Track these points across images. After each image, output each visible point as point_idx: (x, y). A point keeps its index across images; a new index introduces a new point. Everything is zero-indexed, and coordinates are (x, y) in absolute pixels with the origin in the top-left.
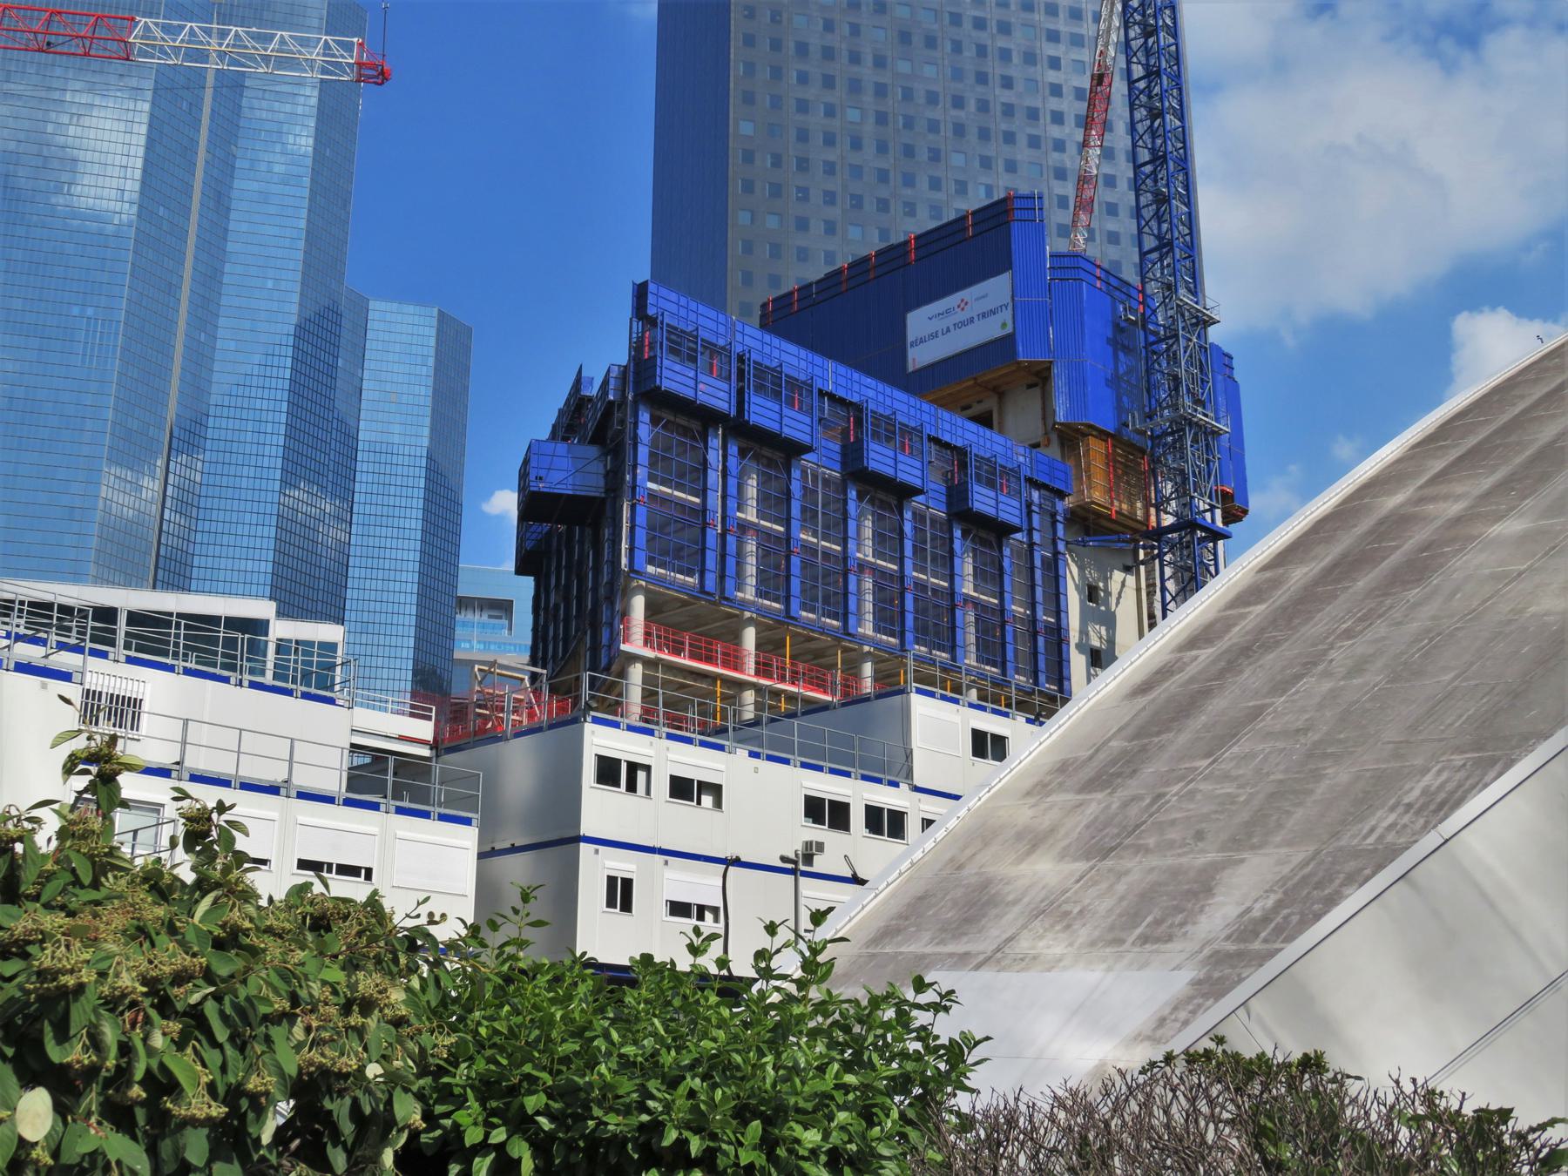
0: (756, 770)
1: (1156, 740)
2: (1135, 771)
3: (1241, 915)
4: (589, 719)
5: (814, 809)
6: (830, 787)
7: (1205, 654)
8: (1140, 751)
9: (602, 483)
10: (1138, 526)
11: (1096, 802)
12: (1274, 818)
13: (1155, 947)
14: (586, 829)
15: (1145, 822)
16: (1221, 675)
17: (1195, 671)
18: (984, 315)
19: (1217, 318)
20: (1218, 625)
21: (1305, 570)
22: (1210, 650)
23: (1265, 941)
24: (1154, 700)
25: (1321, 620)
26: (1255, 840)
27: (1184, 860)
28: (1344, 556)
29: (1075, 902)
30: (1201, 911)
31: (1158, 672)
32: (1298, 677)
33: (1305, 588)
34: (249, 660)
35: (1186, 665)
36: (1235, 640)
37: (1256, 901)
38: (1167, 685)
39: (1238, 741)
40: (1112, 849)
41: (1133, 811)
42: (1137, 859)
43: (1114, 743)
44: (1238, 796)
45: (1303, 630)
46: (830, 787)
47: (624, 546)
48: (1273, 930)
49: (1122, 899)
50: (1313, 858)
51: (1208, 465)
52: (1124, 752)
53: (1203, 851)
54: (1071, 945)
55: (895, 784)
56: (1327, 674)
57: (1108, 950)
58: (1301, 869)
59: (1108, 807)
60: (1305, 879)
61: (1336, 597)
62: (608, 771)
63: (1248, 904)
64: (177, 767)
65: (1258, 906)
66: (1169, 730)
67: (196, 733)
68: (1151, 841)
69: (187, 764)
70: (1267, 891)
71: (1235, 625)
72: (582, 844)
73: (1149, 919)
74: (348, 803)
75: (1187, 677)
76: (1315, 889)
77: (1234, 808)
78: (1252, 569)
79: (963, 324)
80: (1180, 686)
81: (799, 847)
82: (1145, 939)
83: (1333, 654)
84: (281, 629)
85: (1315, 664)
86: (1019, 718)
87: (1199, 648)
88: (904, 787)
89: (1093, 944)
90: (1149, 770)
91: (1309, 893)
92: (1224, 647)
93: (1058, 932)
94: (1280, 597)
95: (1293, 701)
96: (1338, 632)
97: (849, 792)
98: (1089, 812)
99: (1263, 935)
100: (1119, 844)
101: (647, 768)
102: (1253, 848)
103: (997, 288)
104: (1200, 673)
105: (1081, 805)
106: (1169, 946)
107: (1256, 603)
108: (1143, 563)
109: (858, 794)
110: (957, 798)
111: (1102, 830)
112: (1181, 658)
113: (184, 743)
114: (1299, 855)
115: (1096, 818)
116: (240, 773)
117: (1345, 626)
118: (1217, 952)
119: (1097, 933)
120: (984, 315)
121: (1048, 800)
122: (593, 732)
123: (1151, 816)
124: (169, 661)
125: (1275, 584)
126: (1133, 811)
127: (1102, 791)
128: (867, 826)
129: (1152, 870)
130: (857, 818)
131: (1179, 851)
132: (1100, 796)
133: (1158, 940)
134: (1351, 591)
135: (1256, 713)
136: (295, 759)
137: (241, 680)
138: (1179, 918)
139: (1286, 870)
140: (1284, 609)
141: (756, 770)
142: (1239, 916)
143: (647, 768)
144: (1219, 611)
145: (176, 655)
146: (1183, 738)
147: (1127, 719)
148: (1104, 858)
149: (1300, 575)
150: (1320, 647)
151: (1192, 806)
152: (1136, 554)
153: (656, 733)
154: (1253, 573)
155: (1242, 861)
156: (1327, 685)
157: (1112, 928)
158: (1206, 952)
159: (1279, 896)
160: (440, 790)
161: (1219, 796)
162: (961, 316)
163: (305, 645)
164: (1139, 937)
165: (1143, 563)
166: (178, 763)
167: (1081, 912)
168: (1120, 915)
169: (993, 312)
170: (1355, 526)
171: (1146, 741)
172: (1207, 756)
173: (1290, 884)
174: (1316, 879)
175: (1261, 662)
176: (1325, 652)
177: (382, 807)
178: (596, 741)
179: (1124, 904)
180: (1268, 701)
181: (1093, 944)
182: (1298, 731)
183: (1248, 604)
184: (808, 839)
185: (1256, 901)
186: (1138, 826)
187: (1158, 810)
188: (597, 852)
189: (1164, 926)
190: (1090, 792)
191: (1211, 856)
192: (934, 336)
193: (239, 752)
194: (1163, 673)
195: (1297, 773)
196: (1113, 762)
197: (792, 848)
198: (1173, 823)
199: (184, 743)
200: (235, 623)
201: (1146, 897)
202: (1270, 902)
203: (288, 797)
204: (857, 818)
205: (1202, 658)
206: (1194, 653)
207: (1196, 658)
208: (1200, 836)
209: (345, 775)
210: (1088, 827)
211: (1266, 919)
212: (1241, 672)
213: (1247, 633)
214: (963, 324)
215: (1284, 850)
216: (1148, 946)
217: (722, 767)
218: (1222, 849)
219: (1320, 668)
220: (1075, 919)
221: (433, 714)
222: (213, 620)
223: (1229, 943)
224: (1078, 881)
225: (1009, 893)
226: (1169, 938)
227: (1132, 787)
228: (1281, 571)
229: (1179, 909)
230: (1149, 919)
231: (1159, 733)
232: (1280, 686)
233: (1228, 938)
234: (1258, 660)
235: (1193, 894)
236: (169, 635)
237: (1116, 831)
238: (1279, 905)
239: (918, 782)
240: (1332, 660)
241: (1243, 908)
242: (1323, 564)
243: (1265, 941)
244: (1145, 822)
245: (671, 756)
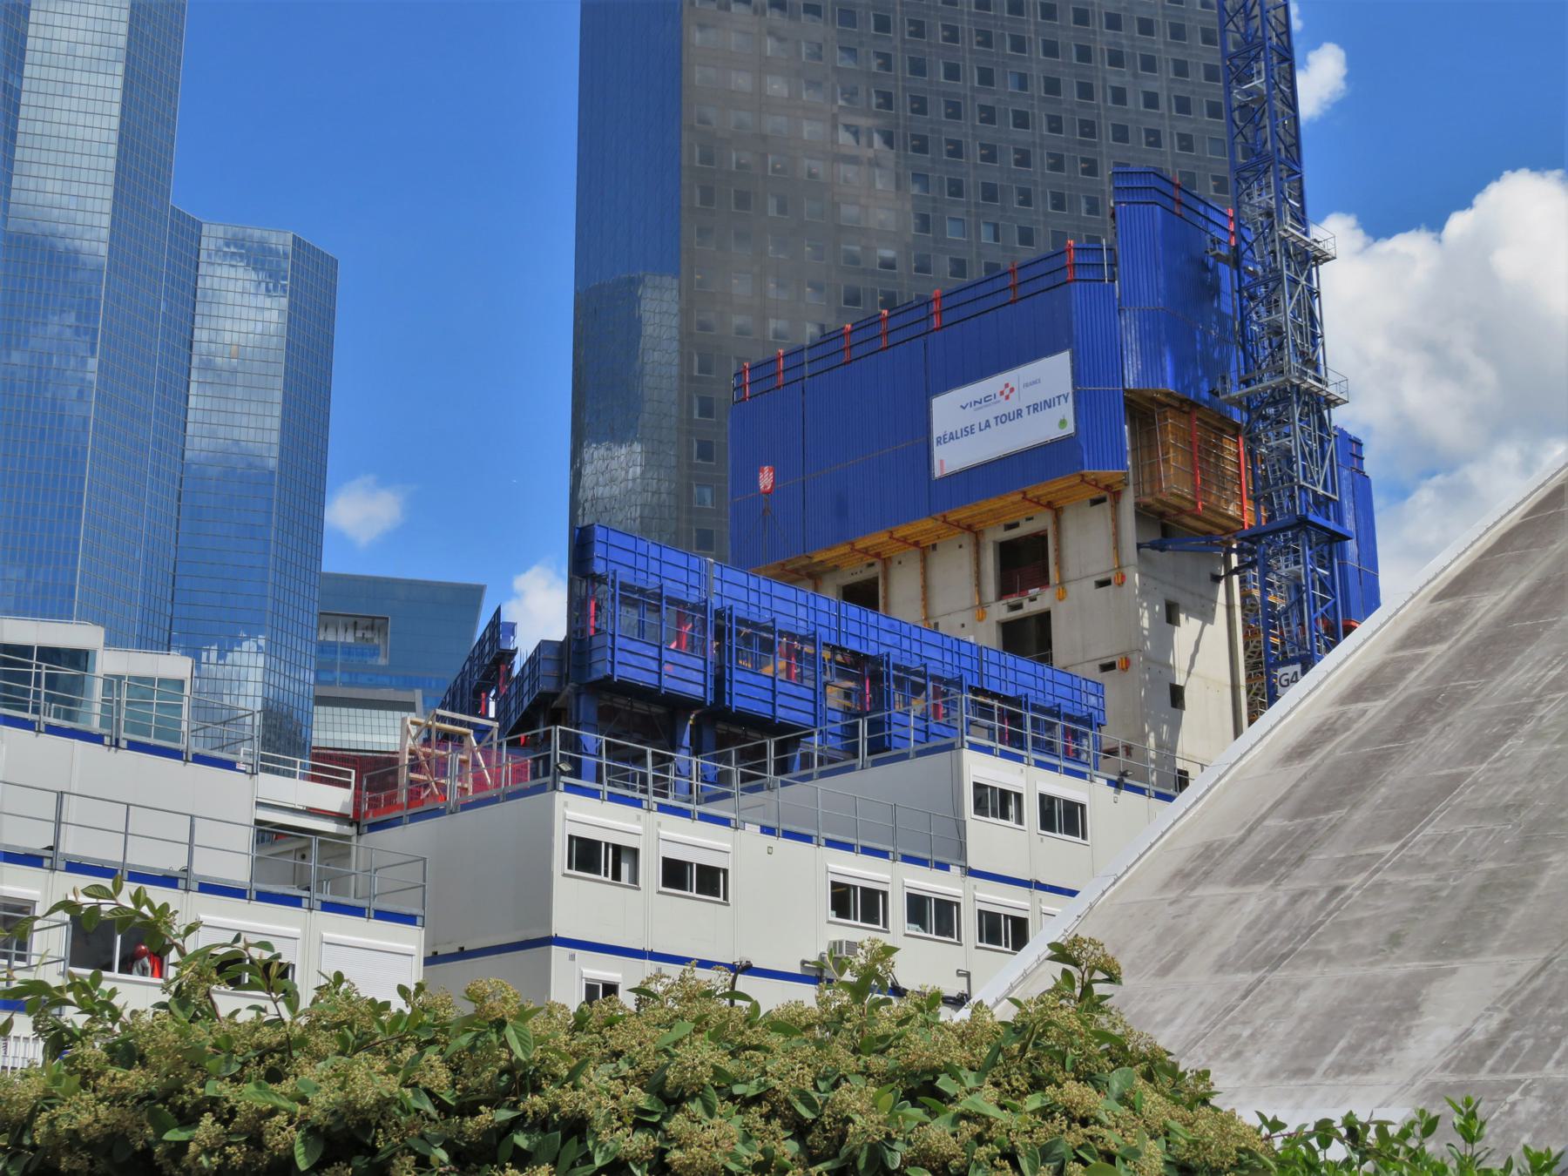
0: (770, 851)
1: (1325, 818)
2: (1302, 858)
3: (1460, 1038)
4: (561, 787)
5: (842, 899)
6: (860, 870)
7: (1376, 708)
8: (1304, 833)
10: (1232, 524)
11: (1256, 899)
12: (1489, 917)
13: (1353, 1078)
14: (559, 928)
15: (1322, 923)
16: (1400, 734)
17: (1365, 729)
18: (1036, 408)
19: (1332, 252)
20: (1388, 670)
21: (1495, 598)
22: (1381, 703)
23: (1493, 1070)
24: (1316, 767)
25: (1521, 665)
26: (1467, 945)
27: (1378, 970)
28: (1544, 582)
29: (1244, 1023)
30: (1408, 1033)
31: (1316, 731)
32: (1502, 738)
33: (1497, 624)
34: (50, 698)
35: (1351, 721)
36: (1413, 690)
37: (1476, 1021)
38: (1329, 747)
39: (1432, 820)
40: (1284, 957)
41: (1306, 906)
42: (1318, 969)
43: (1269, 822)
44: (1440, 890)
45: (1499, 678)
48: (1503, 1056)
49: (1303, 1019)
50: (1543, 968)
51: (1322, 446)
52: (1284, 834)
53: (1401, 959)
54: (1244, 1076)
55: (944, 867)
56: (1536, 736)
57: (1293, 1082)
58: (1530, 981)
59: (1273, 902)
60: (1536, 993)
61: (1538, 635)
62: (586, 855)
63: (1465, 1026)
64: (49, 853)
65: (1480, 1027)
66: (1339, 805)
67: (74, 809)
68: (1333, 947)
69: (61, 850)
70: (1488, 1009)
71: (1410, 669)
72: (554, 947)
73: (1342, 1044)
74: (264, 897)
75: (1355, 737)
76: (1550, 1006)
77: (1435, 904)
78: (1426, 596)
79: (1003, 419)
80: (1349, 749)
81: (824, 949)
82: (1339, 1069)
83: (1542, 710)
84: (109, 662)
85: (1521, 722)
86: (1098, 780)
87: (1367, 700)
88: (955, 870)
89: (1272, 1075)
90: (1322, 858)
91: (1542, 1012)
92: (1400, 699)
93: (1227, 1060)
94: (1466, 634)
95: (1497, 770)
96: (1546, 681)
97: (886, 877)
98: (1248, 909)
99: (1489, 1063)
100: (1293, 951)
101: (634, 852)
102: (1465, 955)
104: (1374, 730)
105: (1236, 900)
106: (1371, 1077)
107: (1434, 642)
108: (1236, 571)
110: (1073, 893)
111: (1267, 932)
112: (1343, 714)
113: (58, 822)
114: (1528, 962)
115: (1259, 918)
116: (128, 861)
117: (1554, 673)
118: (1433, 1085)
119: (1276, 1062)
120: (1036, 408)
121: (1195, 893)
122: (566, 804)
123: (1329, 914)
124: (29, 716)
125: (1457, 616)
126: (1306, 906)
127: (1261, 882)
128: (833, 908)
129: (1338, 982)
130: (969, 925)
131: (1371, 959)
132: (1259, 889)
133: (1355, 1070)
134: (1556, 627)
135: (1451, 785)
136: (196, 842)
137: (117, 741)
138: (1380, 1043)
139: (1510, 982)
140: (1471, 650)
141: (770, 851)
142: (1455, 1041)
143: (634, 852)
144: (1387, 653)
145: (36, 710)
146: (1359, 816)
147: (1283, 791)
148: (1275, 967)
149: (1489, 605)
150: (1525, 700)
151: (1380, 903)
152: (1227, 561)
153: (645, 804)
154: (1426, 603)
155: (1454, 971)
156: (1539, 749)
157: (1295, 1055)
158: (1420, 1084)
159: (1505, 1014)
161: (1415, 889)
163: (142, 684)
164: (1331, 1067)
165: (1236, 571)
166: (51, 848)
167: (1252, 1035)
168: (1304, 1040)
169: (1048, 404)
170: (1552, 542)
171: (1311, 819)
172: (1393, 839)
173: (1517, 1000)
174: (1550, 994)
175: (1449, 719)
176: (1531, 708)
177: (305, 903)
178: (570, 814)
179: (1307, 1025)
180: (1463, 769)
181: (1272, 1075)
182: (1507, 807)
183: (1425, 643)
184: (836, 938)
185: (1476, 1021)
186: (1313, 928)
187: (1338, 908)
188: (572, 957)
189: (1361, 1054)
190: (1246, 884)
191: (1414, 966)
193: (126, 834)
194: (1323, 733)
195: (1512, 861)
196: (1273, 846)
197: (814, 950)
198: (1358, 924)
199: (58, 822)
200: (50, 654)
201: (1336, 1017)
202: (1495, 1023)
203: (187, 890)
204: (969, 925)
205: (1371, 713)
206: (1361, 705)
207: (1365, 712)
208: (1395, 940)
209: (985, 945)
210: (1249, 928)
211: (1491, 1044)
212: (1426, 731)
213: (1428, 680)
214: (1003, 419)
215: (1504, 959)
216: (1344, 1078)
217: (727, 846)
218: (1428, 955)
219: (1528, 727)
220: (1245, 1044)
221: (353, 780)
222: (25, 650)
223: (1447, 1073)
224: (1244, 997)
225: (1156, 1012)
226: (1370, 1068)
227: (1301, 879)
228: (1462, 600)
229: (1377, 1032)
230: (1342, 1044)
231: (1327, 810)
232: (1480, 749)
233: (1445, 1067)
234: (1445, 716)
235: (1394, 1014)
237: (1285, 934)
238: (1506, 1026)
239: (973, 863)
240: (1542, 718)
241: (1460, 1030)
242: (1515, 593)
243: (1493, 1070)
244: (1322, 923)
245: (664, 833)
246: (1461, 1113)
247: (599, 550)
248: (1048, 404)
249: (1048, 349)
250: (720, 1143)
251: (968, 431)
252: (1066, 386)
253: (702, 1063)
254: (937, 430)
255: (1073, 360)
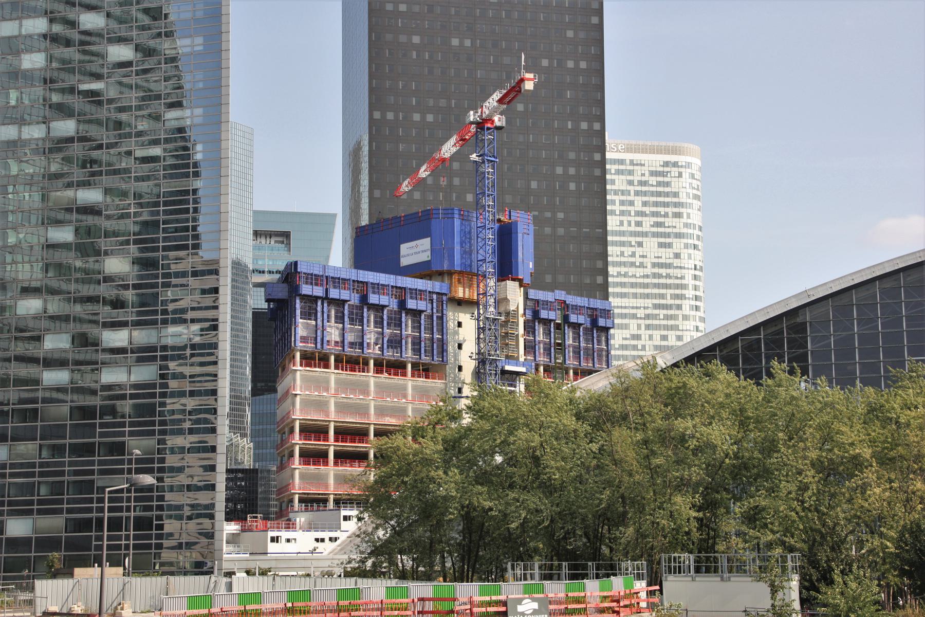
5: (317, 540)
6: (320, 535)
9: (287, 294)
18: (423, 251)
46: (320, 535)
47: (293, 339)
79: (416, 253)
103: (425, 243)
109: (326, 535)
120: (423, 251)
160: (102, 435)
162: (417, 250)
169: (425, 251)
192: (408, 255)
204: (327, 540)
214: (416, 253)
236: (136, 537)
246: (638, 370)
247: (299, 266)
248: (425, 251)
249: (427, 237)
250: (438, 427)
251: (408, 255)
252: (429, 247)
253: (727, 455)
254: (402, 253)
255: (431, 240)
